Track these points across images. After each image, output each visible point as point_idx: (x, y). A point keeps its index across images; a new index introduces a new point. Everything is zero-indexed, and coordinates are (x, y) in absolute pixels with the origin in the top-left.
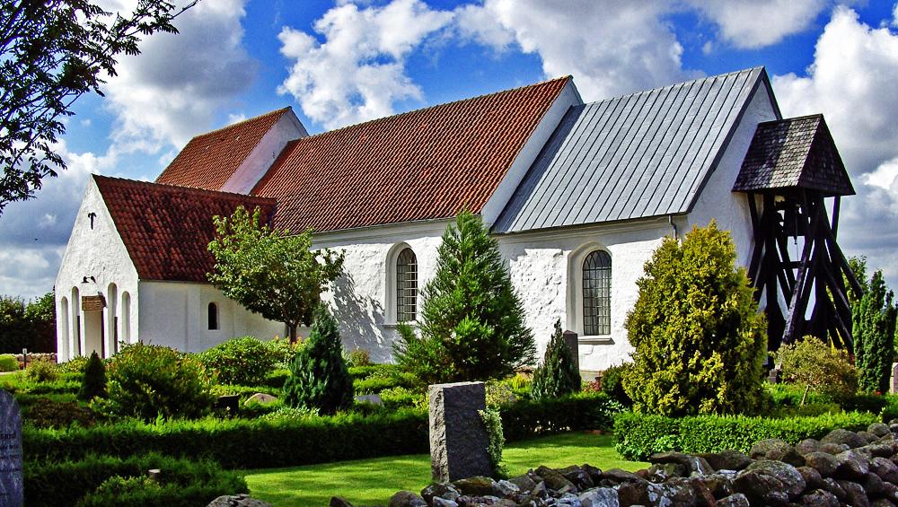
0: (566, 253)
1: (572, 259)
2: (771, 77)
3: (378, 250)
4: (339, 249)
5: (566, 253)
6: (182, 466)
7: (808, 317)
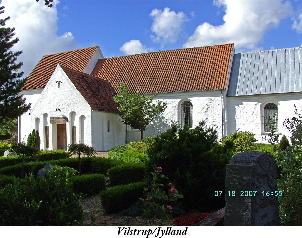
0: (260, 104)
1: (261, 106)
2: (122, 52)
3: (173, 101)
4: (164, 101)
5: (260, 104)
6: (112, 169)
7: (143, 192)
